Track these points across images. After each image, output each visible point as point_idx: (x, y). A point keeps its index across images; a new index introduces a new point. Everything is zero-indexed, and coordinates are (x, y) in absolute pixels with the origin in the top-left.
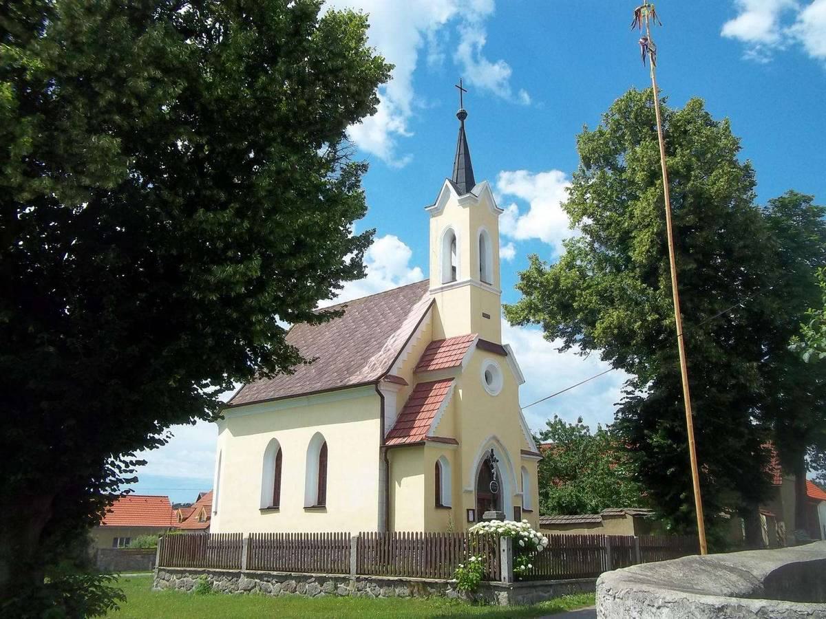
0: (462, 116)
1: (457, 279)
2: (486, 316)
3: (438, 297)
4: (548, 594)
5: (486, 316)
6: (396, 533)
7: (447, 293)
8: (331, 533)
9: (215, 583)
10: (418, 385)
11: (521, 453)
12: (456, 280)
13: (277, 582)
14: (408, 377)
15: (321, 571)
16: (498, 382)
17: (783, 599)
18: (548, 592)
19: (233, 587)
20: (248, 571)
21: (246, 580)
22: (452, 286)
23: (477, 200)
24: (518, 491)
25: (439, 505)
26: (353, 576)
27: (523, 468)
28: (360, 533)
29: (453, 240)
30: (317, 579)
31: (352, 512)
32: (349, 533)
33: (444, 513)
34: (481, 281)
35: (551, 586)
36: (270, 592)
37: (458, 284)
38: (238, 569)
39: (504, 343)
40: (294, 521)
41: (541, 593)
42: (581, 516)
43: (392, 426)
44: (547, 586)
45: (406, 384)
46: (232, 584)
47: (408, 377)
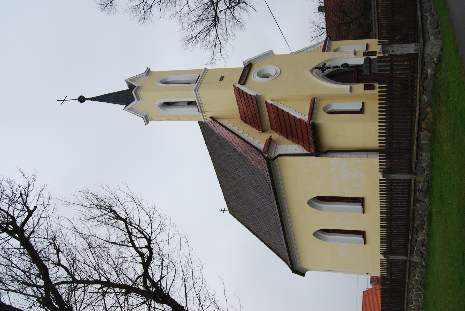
0: (82, 99)
1: (194, 101)
2: (222, 79)
3: (208, 115)
4: (428, 17)
5: (222, 79)
6: (380, 146)
7: (205, 108)
8: (380, 194)
9: (416, 278)
10: (272, 129)
11: (324, 52)
12: (195, 101)
13: (417, 234)
14: (266, 136)
15: (409, 202)
16: (271, 70)
17: (402, 256)
18: (427, 16)
19: (420, 266)
20: (409, 255)
21: (415, 257)
22: (199, 105)
23: (138, 86)
24: (352, 54)
25: (361, 111)
26: (412, 177)
27: (334, 51)
28: (380, 171)
29: (168, 104)
30: (415, 204)
31: (364, 176)
32: (380, 180)
33: (367, 109)
34: (196, 83)
35: (422, 15)
36: (424, 239)
37: (198, 100)
38: (407, 262)
39: (242, 66)
40: (371, 220)
41: (428, 22)
42: (374, 25)
43: (302, 148)
44: (422, 18)
45: (270, 139)
46: (418, 266)
47: (266, 136)
